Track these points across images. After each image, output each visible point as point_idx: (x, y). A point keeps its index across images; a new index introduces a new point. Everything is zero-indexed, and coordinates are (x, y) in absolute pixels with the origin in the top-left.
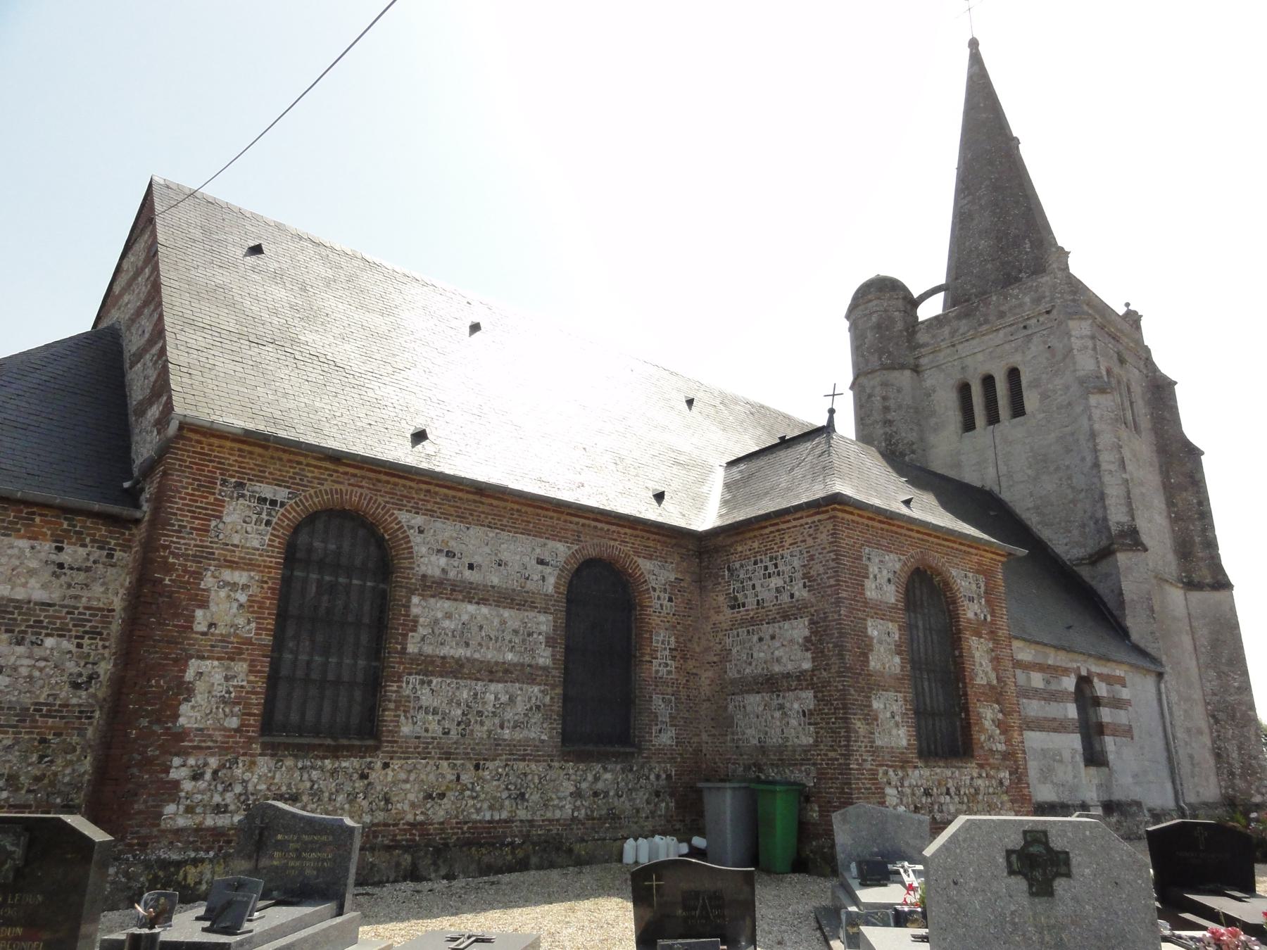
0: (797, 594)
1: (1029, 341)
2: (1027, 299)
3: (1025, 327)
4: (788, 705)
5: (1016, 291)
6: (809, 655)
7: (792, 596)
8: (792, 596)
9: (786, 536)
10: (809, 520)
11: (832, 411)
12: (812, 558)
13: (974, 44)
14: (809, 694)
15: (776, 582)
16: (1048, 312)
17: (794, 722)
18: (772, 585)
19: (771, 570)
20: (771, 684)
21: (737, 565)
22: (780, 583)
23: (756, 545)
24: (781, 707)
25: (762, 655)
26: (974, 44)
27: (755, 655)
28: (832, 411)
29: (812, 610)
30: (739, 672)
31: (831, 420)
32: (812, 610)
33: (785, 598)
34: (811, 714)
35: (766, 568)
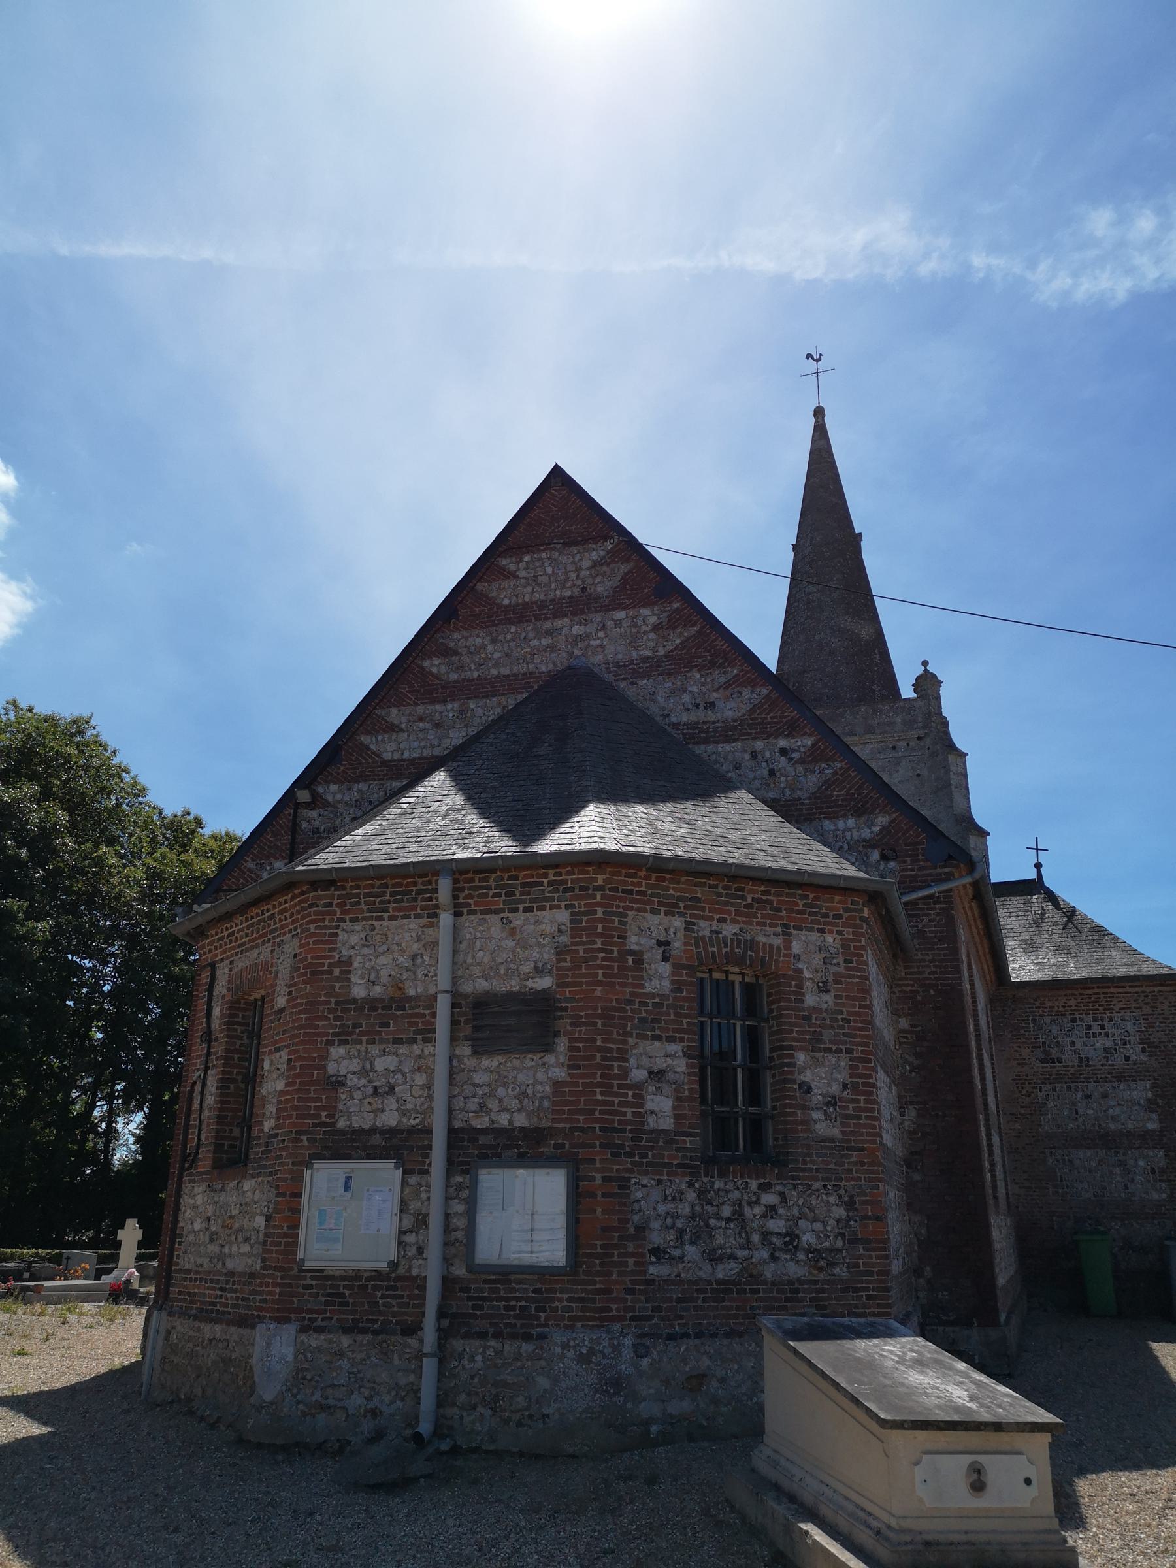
0: (1134, 1057)
1: (898, 764)
2: (899, 720)
3: (894, 748)
4: (1131, 1162)
5: (886, 708)
6: (1154, 1116)
7: (1127, 1058)
8: (1127, 1058)
9: (1115, 1001)
10: (1148, 990)
11: (1038, 866)
12: (1151, 1025)
13: (819, 413)
14: (666, 1123)
15: (1100, 1043)
16: (919, 738)
17: (1139, 1178)
18: (1098, 1045)
19: (1096, 1029)
20: (1109, 1141)
21: (1047, 1019)
22: (1109, 1044)
23: (1073, 1002)
24: (1122, 1163)
25: (1090, 1112)
26: (819, 413)
27: (1081, 1111)
28: (1038, 866)
29: (1156, 1074)
30: (1059, 1127)
31: (1039, 874)
32: (1156, 1074)
33: (1119, 1060)
34: (1163, 1171)
35: (1089, 1028)
